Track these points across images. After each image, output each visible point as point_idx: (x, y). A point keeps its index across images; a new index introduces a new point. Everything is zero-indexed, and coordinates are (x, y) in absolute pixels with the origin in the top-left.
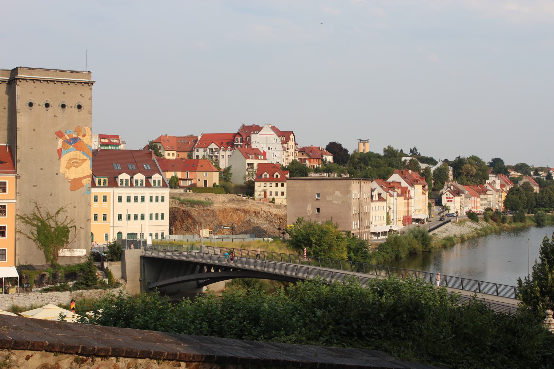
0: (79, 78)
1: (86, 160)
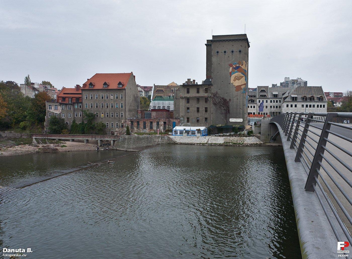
0: (240, 37)
1: (243, 77)
